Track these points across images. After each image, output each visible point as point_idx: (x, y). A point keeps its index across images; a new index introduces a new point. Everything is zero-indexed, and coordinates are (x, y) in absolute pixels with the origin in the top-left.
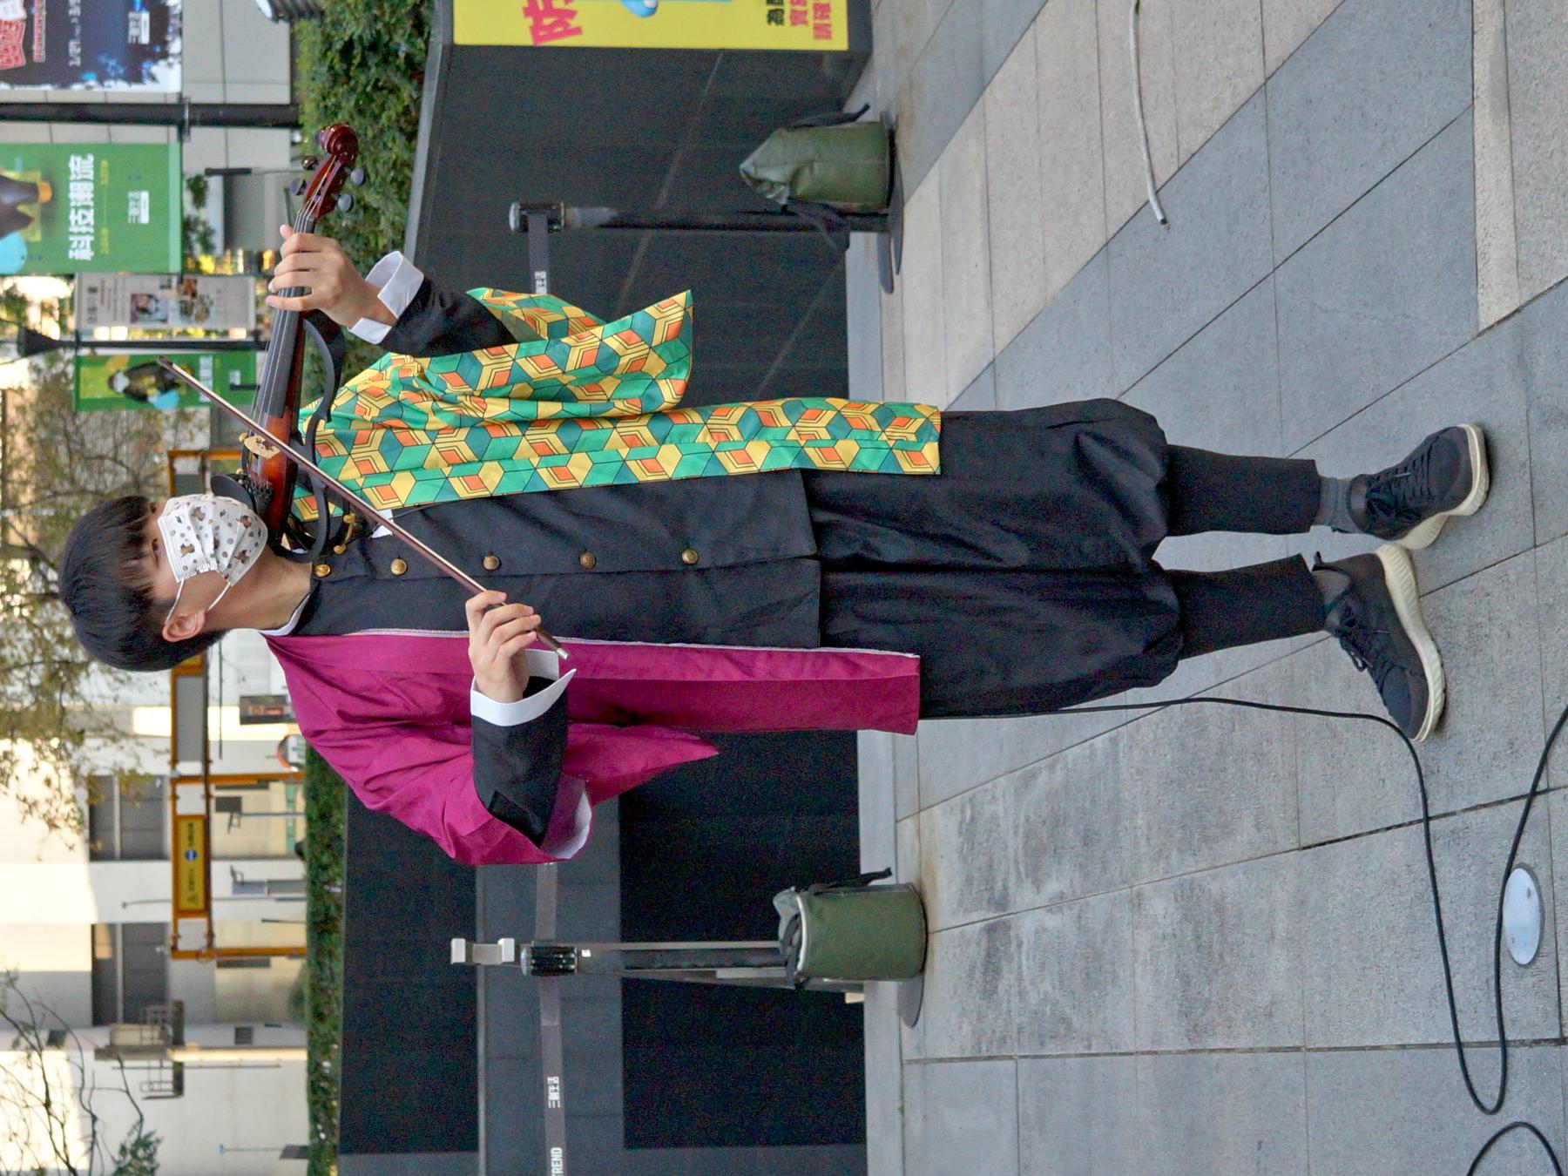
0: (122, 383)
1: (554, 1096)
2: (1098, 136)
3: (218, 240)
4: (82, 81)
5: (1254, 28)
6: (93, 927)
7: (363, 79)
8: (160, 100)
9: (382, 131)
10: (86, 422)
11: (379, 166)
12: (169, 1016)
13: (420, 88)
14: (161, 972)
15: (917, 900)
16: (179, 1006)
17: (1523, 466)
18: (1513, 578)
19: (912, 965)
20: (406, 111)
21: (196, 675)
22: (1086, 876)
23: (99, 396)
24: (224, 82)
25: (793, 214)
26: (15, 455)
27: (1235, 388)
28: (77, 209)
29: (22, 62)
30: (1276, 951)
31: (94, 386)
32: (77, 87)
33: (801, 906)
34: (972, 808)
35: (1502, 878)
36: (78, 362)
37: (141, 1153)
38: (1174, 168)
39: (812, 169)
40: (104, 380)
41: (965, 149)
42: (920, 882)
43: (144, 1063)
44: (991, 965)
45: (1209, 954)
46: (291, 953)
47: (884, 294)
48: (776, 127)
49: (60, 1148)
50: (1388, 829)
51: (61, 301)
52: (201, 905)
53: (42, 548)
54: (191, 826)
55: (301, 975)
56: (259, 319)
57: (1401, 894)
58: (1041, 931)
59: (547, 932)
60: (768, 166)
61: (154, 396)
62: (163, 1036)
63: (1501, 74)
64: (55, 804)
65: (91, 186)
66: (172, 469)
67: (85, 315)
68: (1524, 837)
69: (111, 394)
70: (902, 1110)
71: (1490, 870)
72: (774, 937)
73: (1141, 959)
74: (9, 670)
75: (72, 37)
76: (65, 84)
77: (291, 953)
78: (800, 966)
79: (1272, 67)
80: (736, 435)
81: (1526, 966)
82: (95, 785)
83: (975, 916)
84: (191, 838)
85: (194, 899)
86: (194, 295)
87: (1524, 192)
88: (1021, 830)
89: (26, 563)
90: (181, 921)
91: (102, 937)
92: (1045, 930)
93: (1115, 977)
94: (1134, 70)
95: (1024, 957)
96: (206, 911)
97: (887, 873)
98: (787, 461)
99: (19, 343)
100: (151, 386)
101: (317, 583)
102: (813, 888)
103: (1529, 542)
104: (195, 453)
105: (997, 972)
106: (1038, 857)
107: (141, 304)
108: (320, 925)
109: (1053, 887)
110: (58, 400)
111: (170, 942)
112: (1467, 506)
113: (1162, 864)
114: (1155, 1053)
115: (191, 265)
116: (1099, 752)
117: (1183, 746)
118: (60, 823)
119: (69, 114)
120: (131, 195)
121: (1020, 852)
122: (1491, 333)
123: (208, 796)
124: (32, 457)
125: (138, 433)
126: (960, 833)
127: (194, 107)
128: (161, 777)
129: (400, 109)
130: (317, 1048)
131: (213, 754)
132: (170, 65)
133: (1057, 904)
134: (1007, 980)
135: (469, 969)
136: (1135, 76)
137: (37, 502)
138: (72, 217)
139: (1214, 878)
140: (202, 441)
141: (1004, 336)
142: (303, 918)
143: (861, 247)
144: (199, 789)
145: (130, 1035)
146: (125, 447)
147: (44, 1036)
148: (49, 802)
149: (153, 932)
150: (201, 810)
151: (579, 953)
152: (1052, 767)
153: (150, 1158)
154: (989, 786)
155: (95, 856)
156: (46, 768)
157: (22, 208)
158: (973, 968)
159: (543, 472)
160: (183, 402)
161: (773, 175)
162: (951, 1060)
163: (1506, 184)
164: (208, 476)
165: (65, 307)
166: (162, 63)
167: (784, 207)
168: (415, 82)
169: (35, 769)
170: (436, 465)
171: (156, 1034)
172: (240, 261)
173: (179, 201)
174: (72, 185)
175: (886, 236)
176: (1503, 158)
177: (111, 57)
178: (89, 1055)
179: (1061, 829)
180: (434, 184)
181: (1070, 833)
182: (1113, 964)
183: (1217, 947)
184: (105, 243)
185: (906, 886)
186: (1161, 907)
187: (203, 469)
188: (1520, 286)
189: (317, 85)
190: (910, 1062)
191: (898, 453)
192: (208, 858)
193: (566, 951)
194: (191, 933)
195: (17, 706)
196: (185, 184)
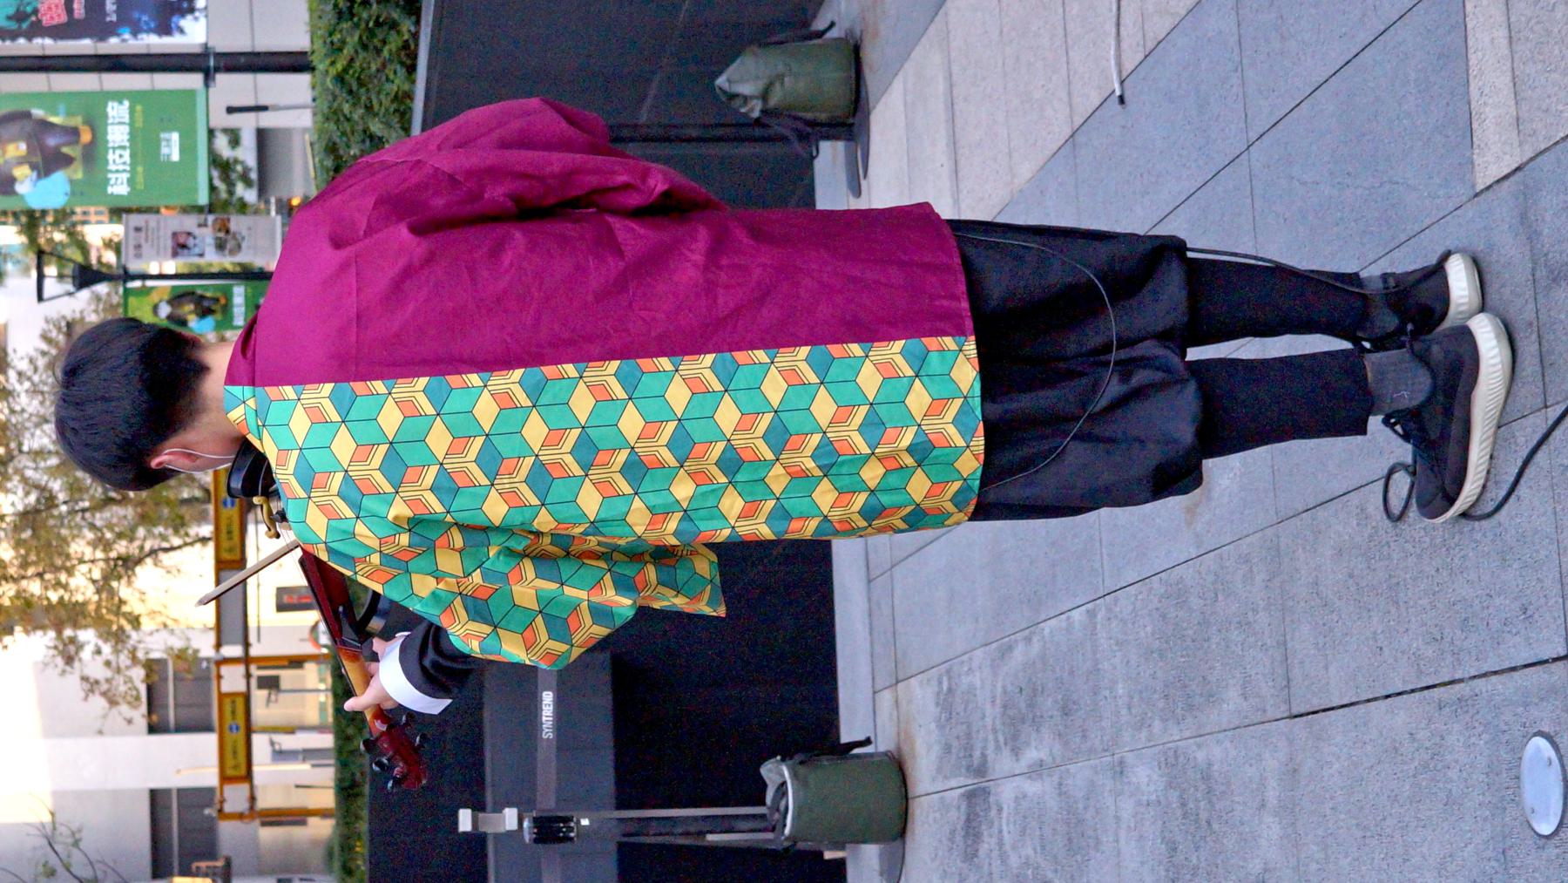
2: (1061, 32)
4: (118, 35)
7: (365, 15)
9: (384, 65)
11: (382, 97)
13: (418, 23)
14: (210, 831)
15: (897, 767)
17: (1531, 324)
19: (894, 829)
20: (406, 46)
22: (1066, 744)
29: (64, 18)
30: (1268, 819)
32: (114, 40)
34: (950, 679)
36: (127, 292)
38: (1141, 56)
39: (782, 84)
41: (927, 58)
42: (899, 749)
44: (972, 829)
45: (1196, 821)
46: (323, 814)
48: (751, 42)
50: (1388, 697)
52: (243, 771)
54: (233, 702)
59: (548, 803)
60: (742, 81)
65: (126, 129)
72: (764, 804)
73: (1124, 826)
77: (323, 814)
78: (787, 831)
81: (1547, 837)
82: (152, 667)
84: (233, 713)
85: (237, 769)
86: (228, 232)
92: (1025, 796)
93: (1098, 842)
95: (1004, 821)
96: (248, 776)
97: (868, 742)
99: (74, 277)
100: (21, 161)
102: (798, 758)
103: (1540, 400)
106: (1018, 723)
107: (182, 240)
108: (347, 790)
109: (1032, 755)
113: (1144, 734)
116: (1076, 624)
117: (1164, 617)
119: (107, 63)
120: (163, 135)
121: (998, 722)
122: (1489, 194)
123: (248, 676)
126: (937, 704)
127: (218, 55)
128: (208, 660)
129: (400, 43)
131: (252, 638)
132: (196, 19)
134: (987, 844)
135: (477, 841)
138: (111, 157)
139: (1199, 746)
142: (332, 784)
144: (241, 669)
149: (195, 798)
151: (578, 822)
152: (1028, 640)
154: (965, 658)
156: (107, 649)
157: (65, 150)
158: (953, 832)
161: (746, 89)
163: (1505, 42)
166: (189, 17)
168: (414, 18)
174: (110, 128)
177: (143, 12)
181: (1049, 702)
183: (1204, 816)
184: (140, 179)
185: (886, 754)
186: (1146, 776)
188: (1521, 144)
192: (249, 731)
193: (567, 820)
194: (235, 797)
195: (80, 598)
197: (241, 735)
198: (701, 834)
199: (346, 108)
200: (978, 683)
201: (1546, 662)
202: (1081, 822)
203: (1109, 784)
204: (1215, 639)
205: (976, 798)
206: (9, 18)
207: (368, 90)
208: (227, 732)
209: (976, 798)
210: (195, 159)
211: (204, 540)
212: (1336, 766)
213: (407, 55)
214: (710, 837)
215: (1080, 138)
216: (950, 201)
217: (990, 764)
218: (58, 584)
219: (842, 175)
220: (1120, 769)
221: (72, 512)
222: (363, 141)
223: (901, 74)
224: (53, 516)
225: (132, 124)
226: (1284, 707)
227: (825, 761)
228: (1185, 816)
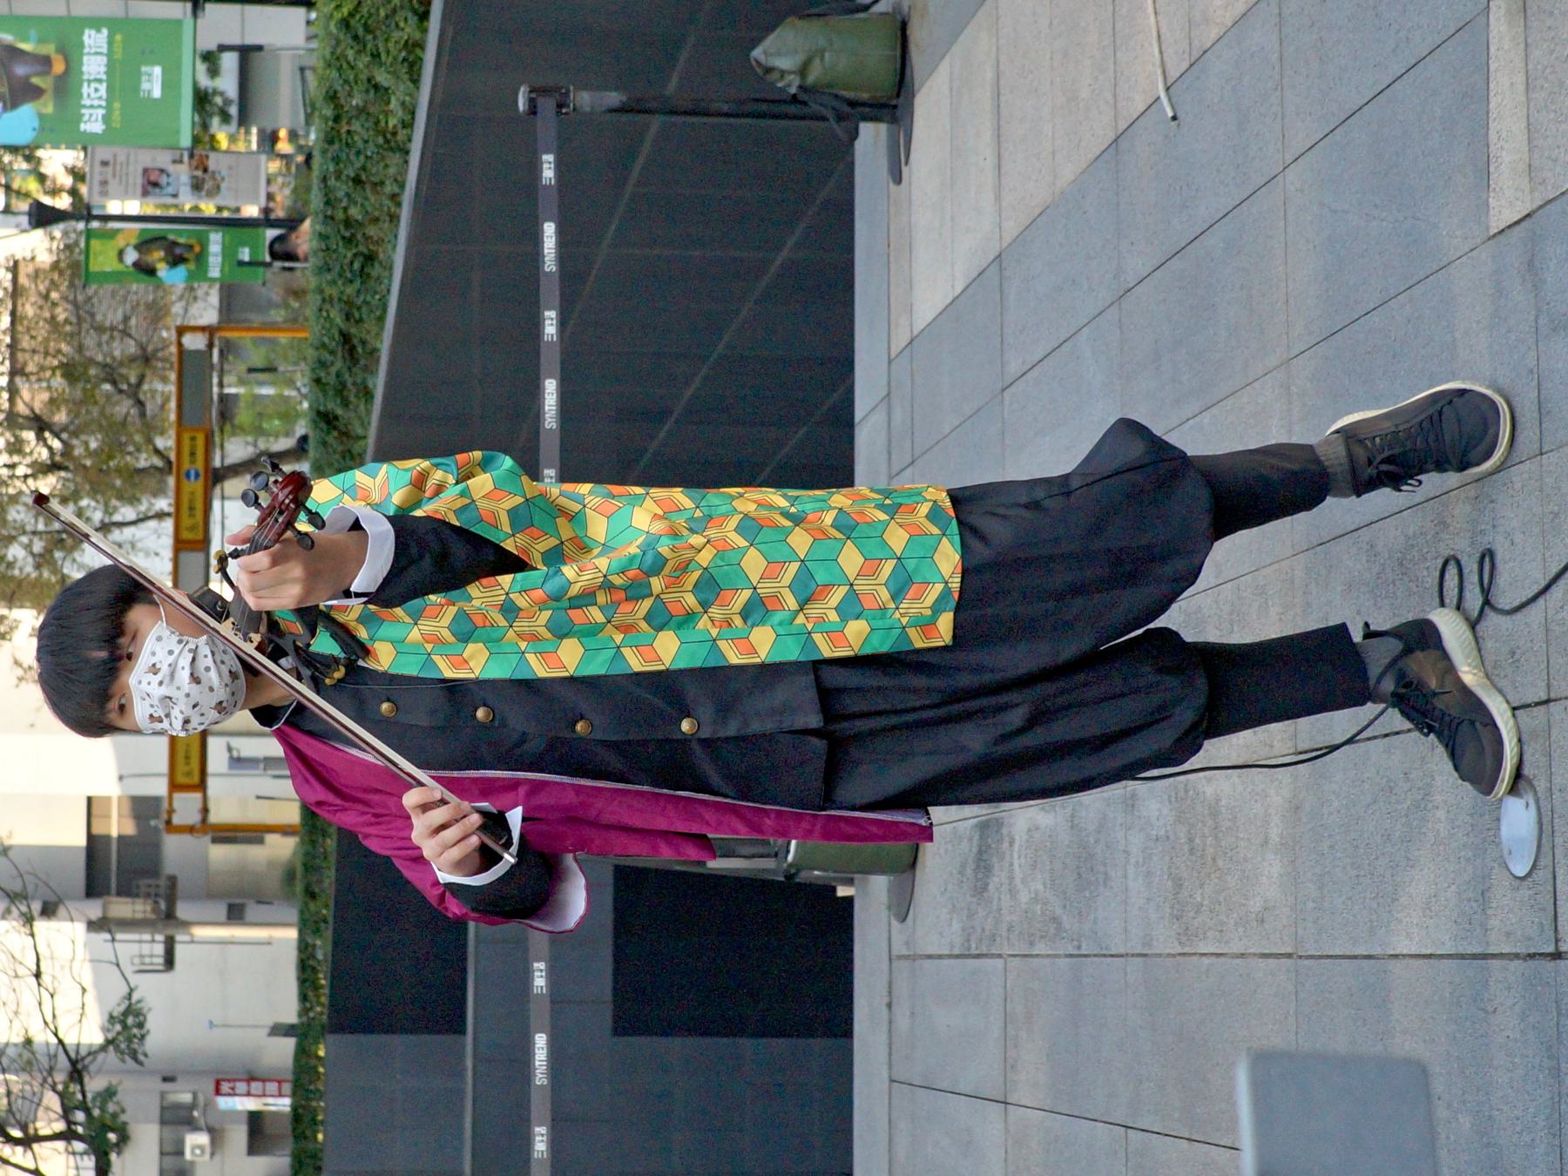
0: (131, 256)
1: (548, 174)
9: (394, 11)
11: (391, 45)
12: (162, 891)
14: (156, 846)
16: (173, 880)
17: (1531, 371)
21: (200, 550)
23: (108, 269)
27: (1242, 287)
28: (89, 81)
31: (104, 259)
36: (89, 234)
37: (130, 1021)
38: (1185, 65)
39: (822, 59)
40: (113, 254)
41: (977, 42)
43: (135, 937)
46: (285, 830)
47: (892, 185)
49: (49, 1019)
50: (1386, 735)
52: (196, 779)
56: (270, 197)
57: (1398, 802)
60: (779, 54)
61: (163, 271)
62: (155, 910)
66: (180, 344)
67: (96, 188)
69: (120, 267)
70: (889, 1005)
73: (1132, 861)
77: (285, 830)
78: (790, 857)
84: (193, 454)
86: (205, 170)
90: (177, 796)
93: (1107, 876)
95: (1016, 855)
96: (202, 786)
100: (160, 260)
104: (203, 329)
105: (988, 869)
107: (153, 178)
110: (73, 268)
111: (165, 816)
114: (1145, 955)
120: (144, 69)
130: (308, 926)
134: (998, 879)
138: (85, 90)
141: (1011, 229)
143: (871, 137)
145: (123, 908)
147: (36, 907)
153: (141, 1025)
157: (35, 80)
158: (963, 866)
160: (191, 276)
161: (784, 63)
162: (940, 957)
163: (1521, 88)
164: (216, 352)
171: (149, 908)
172: (254, 139)
173: (194, 73)
174: (85, 59)
176: (1518, 63)
178: (80, 927)
184: (116, 115)
187: (210, 345)
188: (1532, 191)
190: (900, 957)
194: (186, 808)
199: (350, 54)
201: (1529, 706)
202: (1091, 856)
207: (375, 38)
210: (179, 96)
211: (160, 516)
212: (1336, 804)
215: (1124, 144)
219: (883, 162)
222: (367, 91)
225: (110, 54)
226: (1290, 744)
228: (1192, 851)
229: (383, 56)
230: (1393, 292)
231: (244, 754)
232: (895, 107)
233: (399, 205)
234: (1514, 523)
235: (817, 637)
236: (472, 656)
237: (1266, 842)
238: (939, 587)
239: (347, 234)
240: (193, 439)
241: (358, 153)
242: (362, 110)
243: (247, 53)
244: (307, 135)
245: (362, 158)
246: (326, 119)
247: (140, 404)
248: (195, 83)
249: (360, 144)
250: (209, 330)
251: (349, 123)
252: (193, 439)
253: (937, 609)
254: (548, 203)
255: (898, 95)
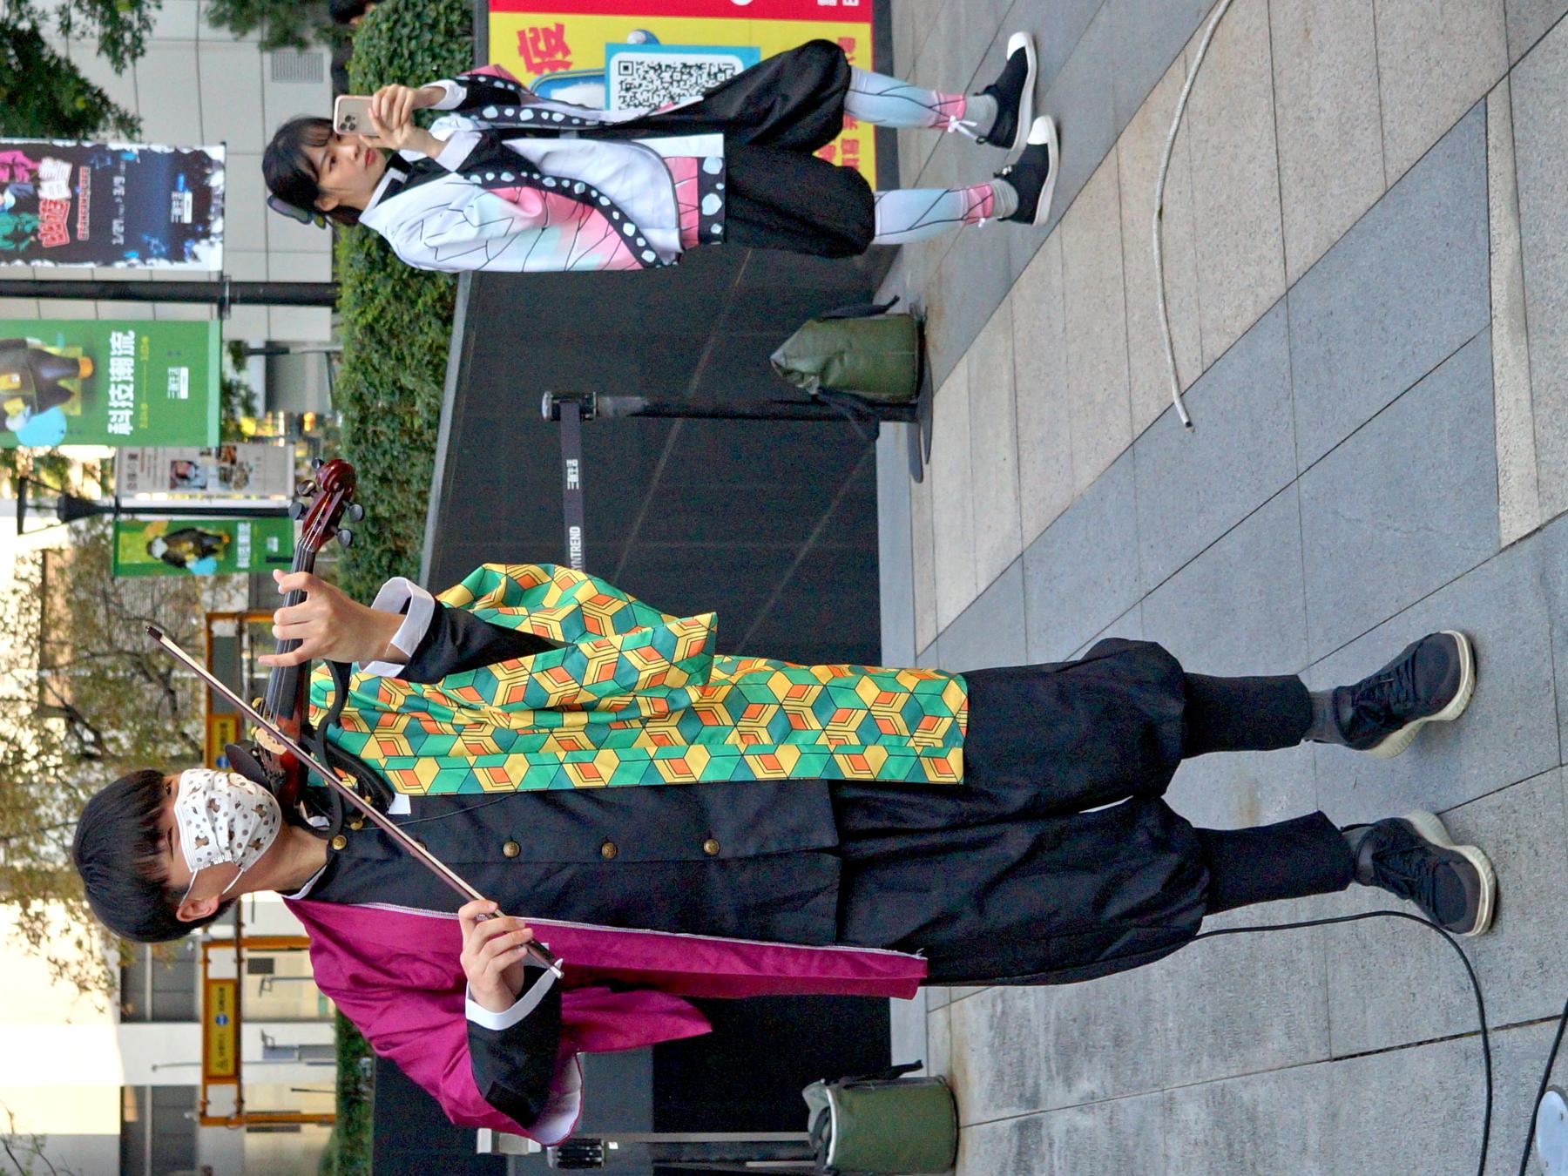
0: (160, 548)
2: (1123, 336)
3: (259, 403)
4: (125, 259)
5: (1275, 239)
6: (122, 1089)
8: (204, 278)
9: (418, 316)
10: (124, 583)
11: (415, 349)
14: (189, 1137)
15: (948, 1092)
17: (1548, 683)
18: (1539, 796)
20: (442, 297)
22: (1116, 1078)
23: (137, 562)
24: (267, 251)
25: (823, 404)
26: (54, 616)
27: (1261, 593)
28: (116, 383)
29: (66, 239)
31: (132, 551)
32: (119, 265)
33: (830, 1099)
34: (1004, 1001)
35: (1535, 1098)
36: (118, 527)
39: (841, 360)
40: (142, 546)
41: (992, 343)
42: (952, 1075)
46: (320, 1120)
48: (806, 317)
50: (1420, 1043)
51: (103, 462)
52: (230, 1070)
53: (78, 708)
55: (331, 1140)
57: (1434, 1111)
58: (1071, 1131)
60: (799, 356)
61: (192, 562)
63: (1518, 293)
64: (86, 966)
66: (210, 631)
67: (125, 481)
68: (1557, 1059)
69: (149, 559)
71: (1523, 1091)
72: (805, 1129)
73: (1173, 1165)
74: (43, 830)
75: (117, 217)
76: (108, 262)
77: (320, 1120)
78: (830, 1160)
79: (1293, 275)
80: (765, 738)
83: (1005, 1113)
84: (221, 1003)
85: (224, 1065)
86: (233, 462)
87: (1544, 412)
88: (1052, 1028)
89: (62, 722)
91: (130, 1101)
94: (1158, 274)
96: (236, 1077)
98: (815, 770)
99: (58, 509)
101: (334, 859)
102: (843, 1081)
103: (1554, 760)
104: (232, 616)
107: (181, 471)
108: (348, 1095)
109: (1085, 1086)
110: (96, 561)
111: (200, 1109)
112: (1451, 711)
113: (1193, 1068)
115: (232, 428)
118: (90, 985)
120: (170, 370)
121: (1052, 1050)
123: (239, 960)
124: (70, 617)
125: (176, 595)
126: (991, 1028)
127: (234, 285)
129: (436, 295)
132: (212, 244)
133: (1087, 1104)
136: (1159, 280)
137: (74, 662)
138: (112, 392)
139: (1246, 1084)
140: (240, 603)
141: (1032, 530)
142: (333, 1088)
143: (892, 437)
144: (231, 952)
146: (163, 610)
148: (80, 964)
150: (232, 974)
151: (606, 1145)
155: (125, 1018)
157: (62, 383)
158: (1004, 1166)
159: (569, 768)
161: (802, 366)
163: (1526, 404)
164: (246, 638)
165: (107, 467)
166: (204, 242)
167: (814, 397)
169: (68, 930)
170: (461, 754)
172: (282, 423)
173: (219, 365)
174: (112, 361)
175: (914, 426)
176: (1523, 379)
177: (153, 236)
179: (1092, 1028)
180: (464, 387)
181: (1102, 1032)
182: (1145, 1169)
184: (144, 417)
185: (936, 1079)
186: (1193, 1113)
187: (240, 631)
188: (1541, 505)
189: (355, 271)
191: (925, 761)
192: (238, 1020)
194: (221, 1099)
195: (50, 867)
196: (225, 348)
197: (229, 1028)
198: (741, 1161)
199: (375, 358)
200: (1032, 1006)
203: (1158, 1120)
204: (1262, 976)
205: (1027, 1129)
206: (6, 238)
208: (213, 1024)
209: (1027, 1129)
213: (444, 308)
214: (750, 1164)
216: (1012, 497)
217: (1042, 1095)
218: (24, 850)
219: (904, 459)
220: (1169, 1106)
221: (44, 769)
223: (965, 359)
224: (20, 773)
225: (137, 357)
226: (1325, 1050)
227: (871, 1085)
229: (408, 361)
230: (1409, 601)
231: (279, 1042)
232: (915, 406)
233: (426, 502)
234: (1538, 834)
235: (839, 758)
236: (512, 768)
237: (1304, 1149)
238: (948, 721)
239: (375, 532)
240: (224, 726)
241: (385, 453)
242: (389, 411)
243: (274, 352)
244: (335, 418)
245: (388, 457)
246: (353, 421)
247: (172, 692)
248: (222, 374)
249: (387, 445)
250: (239, 617)
251: (375, 424)
252: (224, 726)
253: (948, 739)
254: (573, 508)
255: (918, 394)
